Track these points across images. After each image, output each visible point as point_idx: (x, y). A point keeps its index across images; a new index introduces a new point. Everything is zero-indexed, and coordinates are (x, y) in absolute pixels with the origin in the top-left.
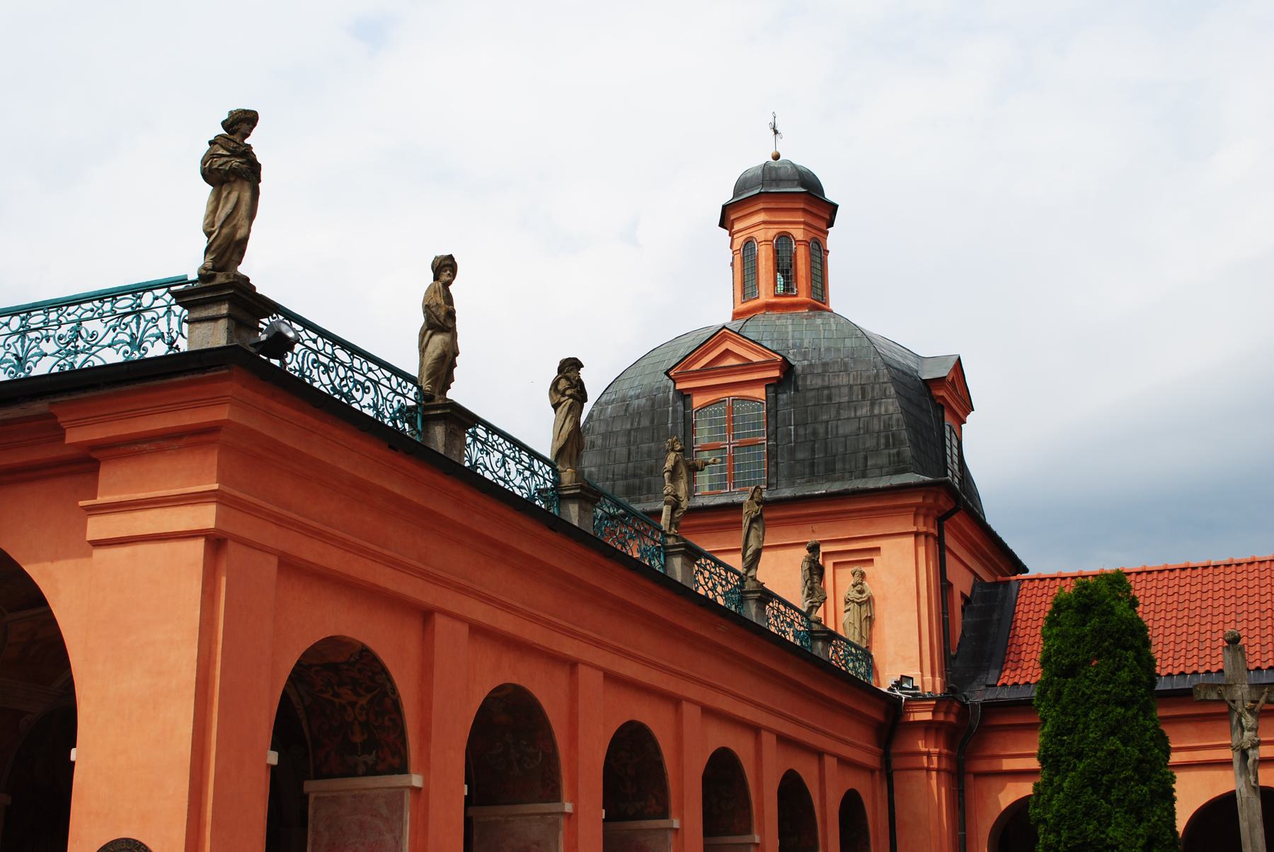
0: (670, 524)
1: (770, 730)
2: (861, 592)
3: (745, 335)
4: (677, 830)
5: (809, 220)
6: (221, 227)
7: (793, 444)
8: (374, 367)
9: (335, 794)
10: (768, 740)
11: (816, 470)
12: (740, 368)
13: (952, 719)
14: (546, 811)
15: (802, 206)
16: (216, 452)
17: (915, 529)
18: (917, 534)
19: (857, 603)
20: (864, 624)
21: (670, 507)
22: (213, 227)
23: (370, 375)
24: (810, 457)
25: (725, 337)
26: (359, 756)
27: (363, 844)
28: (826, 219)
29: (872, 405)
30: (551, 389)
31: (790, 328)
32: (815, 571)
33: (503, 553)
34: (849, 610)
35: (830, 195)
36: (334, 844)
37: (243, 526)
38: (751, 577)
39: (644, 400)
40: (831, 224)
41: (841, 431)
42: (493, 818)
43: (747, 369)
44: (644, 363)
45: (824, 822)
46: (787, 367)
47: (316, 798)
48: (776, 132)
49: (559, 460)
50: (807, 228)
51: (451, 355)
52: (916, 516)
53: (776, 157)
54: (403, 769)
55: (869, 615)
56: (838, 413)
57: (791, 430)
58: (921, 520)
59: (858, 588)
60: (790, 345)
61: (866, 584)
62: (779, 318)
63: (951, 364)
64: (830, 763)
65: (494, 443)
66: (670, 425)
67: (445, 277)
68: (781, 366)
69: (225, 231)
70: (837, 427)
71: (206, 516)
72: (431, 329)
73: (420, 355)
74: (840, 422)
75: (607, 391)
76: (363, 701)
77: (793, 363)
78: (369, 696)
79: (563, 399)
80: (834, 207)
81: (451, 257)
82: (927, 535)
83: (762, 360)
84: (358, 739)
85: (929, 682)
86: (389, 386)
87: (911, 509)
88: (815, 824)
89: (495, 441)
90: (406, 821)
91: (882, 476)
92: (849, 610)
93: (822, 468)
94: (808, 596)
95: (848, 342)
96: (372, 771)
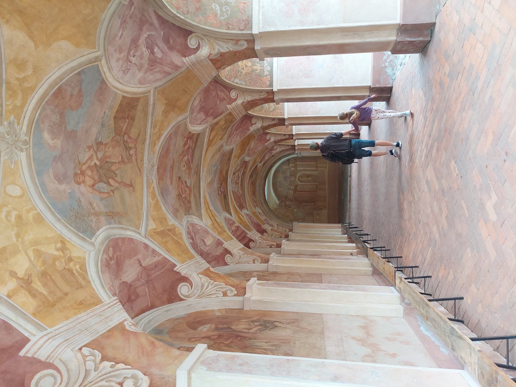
42: (261, 17)
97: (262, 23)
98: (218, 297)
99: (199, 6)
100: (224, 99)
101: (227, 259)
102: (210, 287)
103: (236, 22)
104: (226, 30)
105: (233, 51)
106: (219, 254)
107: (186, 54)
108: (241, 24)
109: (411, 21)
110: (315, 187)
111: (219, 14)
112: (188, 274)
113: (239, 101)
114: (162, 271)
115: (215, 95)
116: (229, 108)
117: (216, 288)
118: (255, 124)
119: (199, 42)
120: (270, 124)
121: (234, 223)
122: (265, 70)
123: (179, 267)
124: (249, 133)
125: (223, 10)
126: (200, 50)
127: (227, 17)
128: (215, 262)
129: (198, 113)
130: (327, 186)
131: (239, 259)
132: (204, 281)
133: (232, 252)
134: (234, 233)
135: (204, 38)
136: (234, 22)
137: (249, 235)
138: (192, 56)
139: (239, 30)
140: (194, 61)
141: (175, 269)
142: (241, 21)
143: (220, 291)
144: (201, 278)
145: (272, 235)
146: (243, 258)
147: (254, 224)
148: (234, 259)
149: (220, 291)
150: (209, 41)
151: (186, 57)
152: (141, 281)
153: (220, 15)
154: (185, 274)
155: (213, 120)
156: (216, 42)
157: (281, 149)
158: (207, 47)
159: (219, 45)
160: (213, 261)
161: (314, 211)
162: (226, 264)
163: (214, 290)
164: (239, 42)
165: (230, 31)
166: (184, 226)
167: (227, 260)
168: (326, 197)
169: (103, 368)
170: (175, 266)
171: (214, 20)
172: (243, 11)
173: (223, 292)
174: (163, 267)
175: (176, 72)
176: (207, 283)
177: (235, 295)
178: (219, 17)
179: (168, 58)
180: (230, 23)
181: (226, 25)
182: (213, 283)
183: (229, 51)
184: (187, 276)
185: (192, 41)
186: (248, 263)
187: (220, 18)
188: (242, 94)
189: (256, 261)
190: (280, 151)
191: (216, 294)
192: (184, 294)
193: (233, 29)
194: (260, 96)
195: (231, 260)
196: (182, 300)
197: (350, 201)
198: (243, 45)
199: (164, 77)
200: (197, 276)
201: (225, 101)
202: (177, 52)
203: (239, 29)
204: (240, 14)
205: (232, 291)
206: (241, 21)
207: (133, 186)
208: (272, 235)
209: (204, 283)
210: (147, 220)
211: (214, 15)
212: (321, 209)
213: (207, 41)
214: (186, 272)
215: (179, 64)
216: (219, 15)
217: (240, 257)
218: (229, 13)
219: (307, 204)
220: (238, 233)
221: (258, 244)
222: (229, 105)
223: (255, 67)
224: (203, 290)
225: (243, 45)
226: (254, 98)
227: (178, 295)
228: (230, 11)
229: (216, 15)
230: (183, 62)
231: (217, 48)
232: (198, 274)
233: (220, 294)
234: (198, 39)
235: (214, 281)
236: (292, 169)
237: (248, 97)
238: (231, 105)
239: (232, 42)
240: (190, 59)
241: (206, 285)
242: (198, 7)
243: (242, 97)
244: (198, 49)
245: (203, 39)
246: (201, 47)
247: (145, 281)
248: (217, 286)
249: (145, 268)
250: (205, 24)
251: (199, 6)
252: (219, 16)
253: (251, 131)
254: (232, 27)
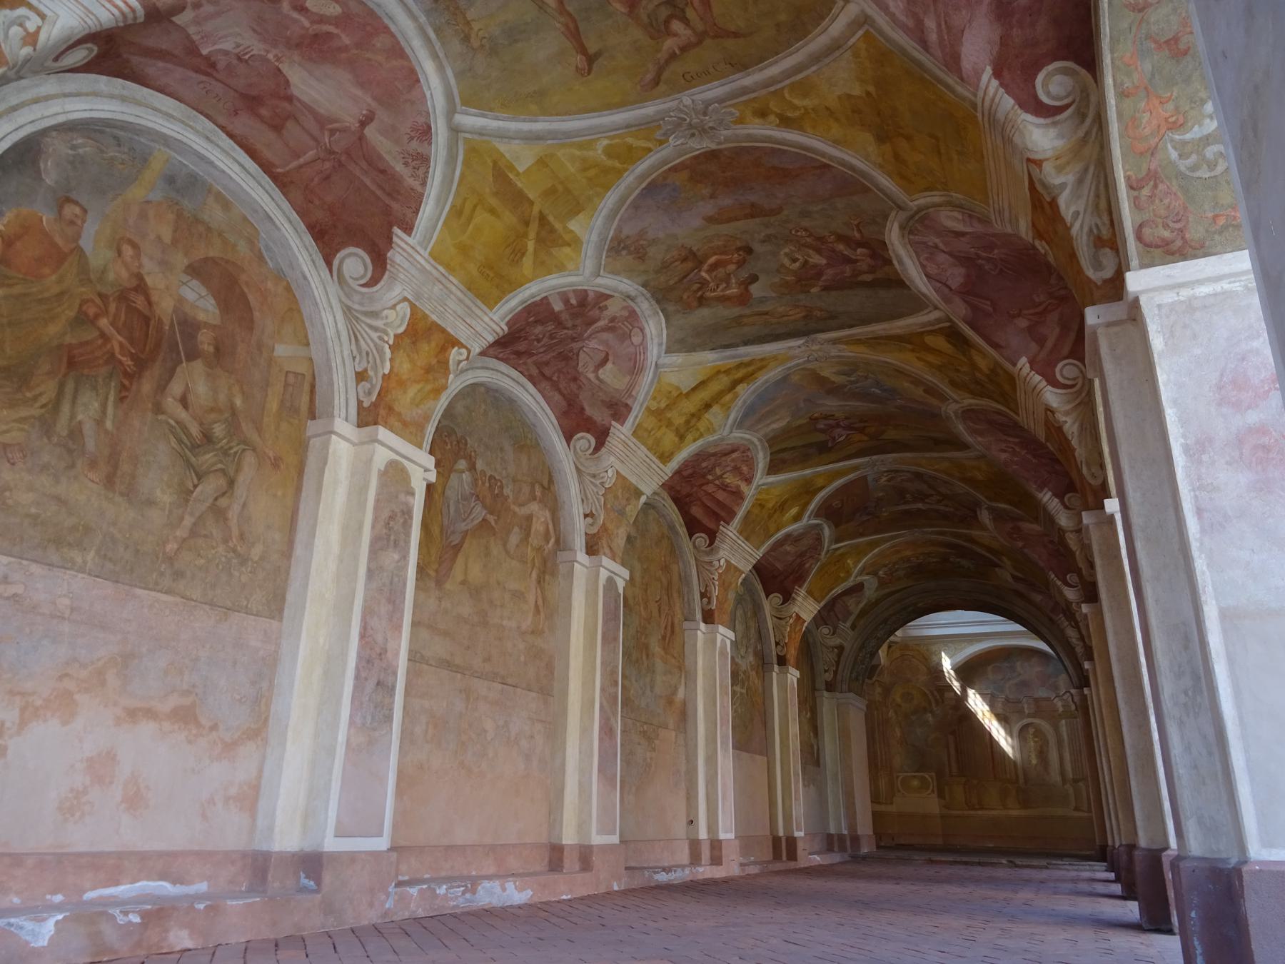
42: (1204, 290)
97: (1180, 298)
98: (354, 361)
99: (1189, 48)
100: (1041, 342)
101: (582, 438)
102: (375, 335)
103: (1169, 207)
104: (1128, 178)
105: (1072, 238)
106: (589, 414)
107: (1006, 73)
108: (1166, 226)
109: (1255, 909)
110: (1008, 776)
111: (1188, 136)
112: (398, 270)
113: (1052, 397)
114: (379, 193)
115: (1041, 304)
116: (1019, 366)
117: (375, 351)
118: (1066, 507)
119: (1067, 107)
120: (1077, 553)
121: (749, 481)
123: (406, 243)
124: (1032, 488)
125: (1209, 148)
126: (1041, 121)
127: (1183, 168)
128: (564, 403)
129: (950, 254)
130: (1015, 813)
131: (589, 474)
132: (387, 317)
133: (603, 450)
134: (717, 482)
135: (1088, 121)
136: (1166, 201)
137: (724, 529)
138: (1008, 102)
139: (1136, 227)
140: (1000, 115)
141: (396, 230)
142: (1178, 226)
143: (368, 362)
144: (394, 307)
145: (780, 619)
146: (595, 486)
147: (798, 561)
148: (587, 459)
149: (368, 362)
150: (1084, 141)
151: (995, 78)
152: (324, 134)
153: (1184, 143)
154: (393, 262)
155: (963, 320)
156: (1086, 170)
157: (1074, 640)
158: (1059, 143)
159: (1080, 181)
160: (563, 395)
161: (933, 774)
162: (569, 437)
163: (369, 346)
164: (1107, 250)
165: (1125, 195)
166: (599, 281)
167: (579, 439)
168: (982, 809)
170: (408, 229)
171: (1155, 122)
172: (1221, 221)
173: (366, 370)
174: (389, 195)
175: (939, 65)
176: (384, 325)
177: (360, 403)
178: (1172, 141)
179: (964, 12)
180: (1161, 187)
181: (1147, 175)
182: (384, 341)
183: (1069, 225)
184: (388, 266)
185: (1058, 78)
186: (583, 501)
187: (1169, 146)
188: (1077, 402)
189: (589, 520)
190: (1070, 640)
191: (360, 353)
192: (345, 268)
193: (1136, 205)
194: (1088, 465)
195: (581, 451)
196: (329, 263)
197: (931, 862)
198: (1098, 266)
199: (904, 28)
200: (400, 298)
201: (1034, 347)
202: (1001, 38)
203: (1141, 226)
204: (1210, 215)
205: (369, 393)
206: (1178, 226)
207: (595, 66)
208: (780, 619)
209: (382, 319)
210: (537, 137)
211: (1178, 119)
212: (941, 795)
213: (1081, 133)
214: (399, 265)
215: (967, 64)
216: (1181, 137)
217: (594, 476)
218: (1204, 173)
219: (953, 752)
220: (721, 496)
221: (707, 559)
222: (1030, 363)
224: (363, 318)
225: (1098, 266)
226: (1074, 443)
227: (338, 251)
228: (1212, 174)
229: (1176, 127)
230: (978, 75)
231: (1068, 178)
232: (405, 299)
233: (359, 364)
234: (1077, 100)
235: (391, 342)
236: (1059, 704)
237: (1074, 423)
238: (1032, 369)
239: (1104, 224)
240: (997, 100)
241: (379, 323)
242: (1182, 46)
243: (1069, 402)
244: (1040, 109)
245: (1082, 116)
246: (1049, 121)
247: (328, 145)
248: (378, 352)
249: (361, 138)
250: (1122, 94)
251: (1189, 48)
252: (1177, 137)
253: (1040, 495)
254: (1143, 199)
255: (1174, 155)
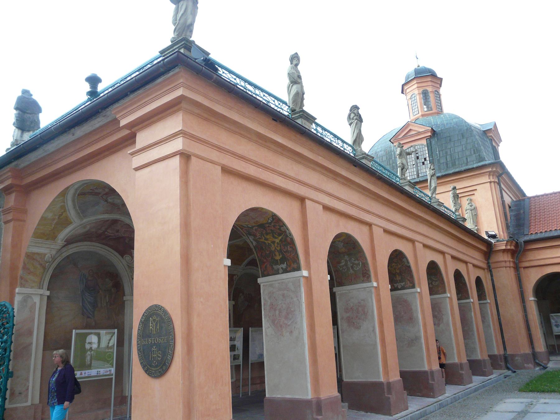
0: (402, 175)
1: (448, 254)
2: (471, 206)
3: (416, 123)
4: (419, 292)
5: (433, 84)
6: (180, 20)
7: (439, 158)
8: (266, 95)
9: (271, 283)
10: (448, 257)
11: (448, 166)
12: (416, 134)
13: (513, 248)
14: (366, 286)
15: (430, 80)
16: (181, 114)
17: (489, 181)
18: (490, 182)
19: (470, 210)
20: (474, 217)
21: (401, 168)
22: (176, 21)
23: (264, 98)
24: (446, 161)
25: (409, 125)
26: (279, 265)
27: (285, 303)
28: (439, 84)
29: (467, 140)
30: (348, 118)
31: (432, 119)
32: (456, 197)
33: (335, 176)
34: (467, 213)
35: (439, 75)
36: (272, 305)
37: (196, 149)
38: (434, 197)
39: (383, 152)
40: (441, 86)
41: (456, 151)
42: (344, 292)
43: (418, 135)
44: (381, 140)
45: (471, 288)
46: (433, 132)
47: (263, 286)
48: (417, 58)
49: (354, 145)
50: (433, 87)
51: (302, 94)
52: (489, 176)
53: (419, 66)
54: (298, 269)
55: (475, 214)
56: (454, 144)
57: (437, 153)
58: (491, 177)
59: (470, 204)
60: (433, 124)
61: (473, 203)
62: (427, 118)
63: (493, 124)
64: (470, 266)
65: (326, 135)
66: (393, 158)
67: (295, 62)
68: (431, 131)
69: (182, 21)
70: (454, 150)
71: (178, 144)
72: (292, 83)
73: (288, 95)
74: (455, 147)
75: (370, 151)
76: (277, 241)
77: (435, 130)
78: (280, 238)
79: (353, 121)
80: (441, 79)
81: (296, 53)
82: (494, 182)
83: (424, 130)
84: (278, 257)
85: (503, 235)
86: (274, 104)
87: (486, 174)
88: (467, 289)
89: (326, 134)
90: (302, 292)
91: (474, 164)
92: (467, 213)
93: (451, 165)
94: (454, 206)
95: (454, 120)
96: (285, 271)
122: (398, 284)
169: (424, 72)
218: (343, 271)
223: (397, 276)
255: (339, 268)
